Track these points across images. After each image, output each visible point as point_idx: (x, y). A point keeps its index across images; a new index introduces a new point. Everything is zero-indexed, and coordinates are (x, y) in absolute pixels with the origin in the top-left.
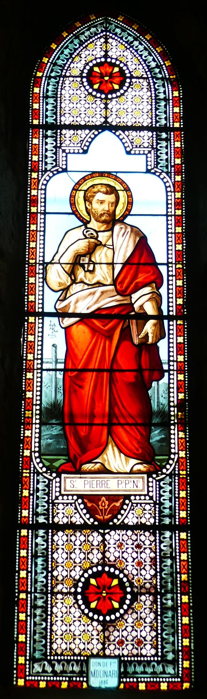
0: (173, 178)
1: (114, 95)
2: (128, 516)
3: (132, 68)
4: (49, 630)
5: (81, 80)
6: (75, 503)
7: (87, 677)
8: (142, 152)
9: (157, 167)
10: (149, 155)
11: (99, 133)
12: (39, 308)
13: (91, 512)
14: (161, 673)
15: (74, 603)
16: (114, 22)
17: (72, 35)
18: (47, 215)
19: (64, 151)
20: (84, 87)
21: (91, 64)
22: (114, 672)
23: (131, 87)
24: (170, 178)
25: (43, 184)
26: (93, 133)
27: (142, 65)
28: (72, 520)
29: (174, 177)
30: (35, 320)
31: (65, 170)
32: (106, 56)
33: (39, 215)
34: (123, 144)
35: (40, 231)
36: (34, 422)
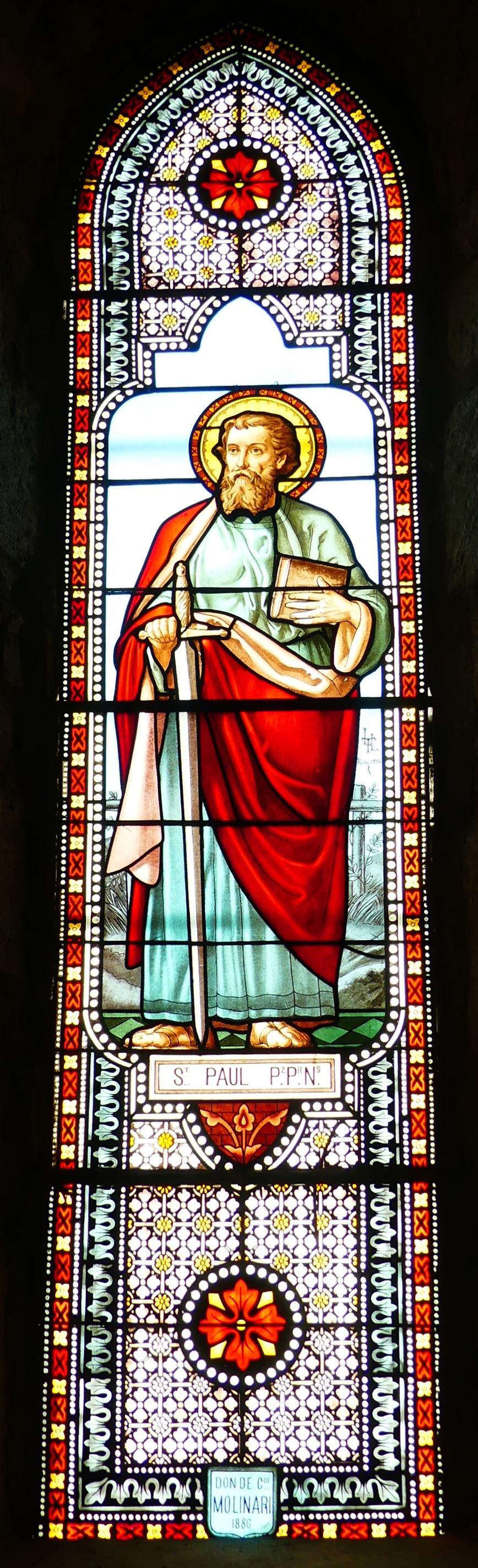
0: (388, 396)
1: (256, 223)
2: (297, 1150)
3: (294, 158)
4: (118, 1411)
5: (304, 1314)
6: (300, 332)
7: (205, 1513)
8: (320, 341)
9: (123, 1069)
10: (336, 348)
11: (224, 304)
12: (94, 693)
13: (215, 1138)
14: (370, 1501)
15: (297, 167)
16: (255, 55)
17: (165, 90)
18: (111, 489)
19: (146, 347)
20: (297, 1298)
21: (206, 155)
22: (264, 1501)
23: (178, 1302)
24: (383, 395)
25: (101, 419)
26: (211, 306)
27: (319, 153)
28: (307, 302)
29: (392, 393)
30: (87, 718)
31: (152, 389)
32: (239, 135)
33: (93, 485)
34: (279, 325)
35: (96, 522)
36: (90, 613)
